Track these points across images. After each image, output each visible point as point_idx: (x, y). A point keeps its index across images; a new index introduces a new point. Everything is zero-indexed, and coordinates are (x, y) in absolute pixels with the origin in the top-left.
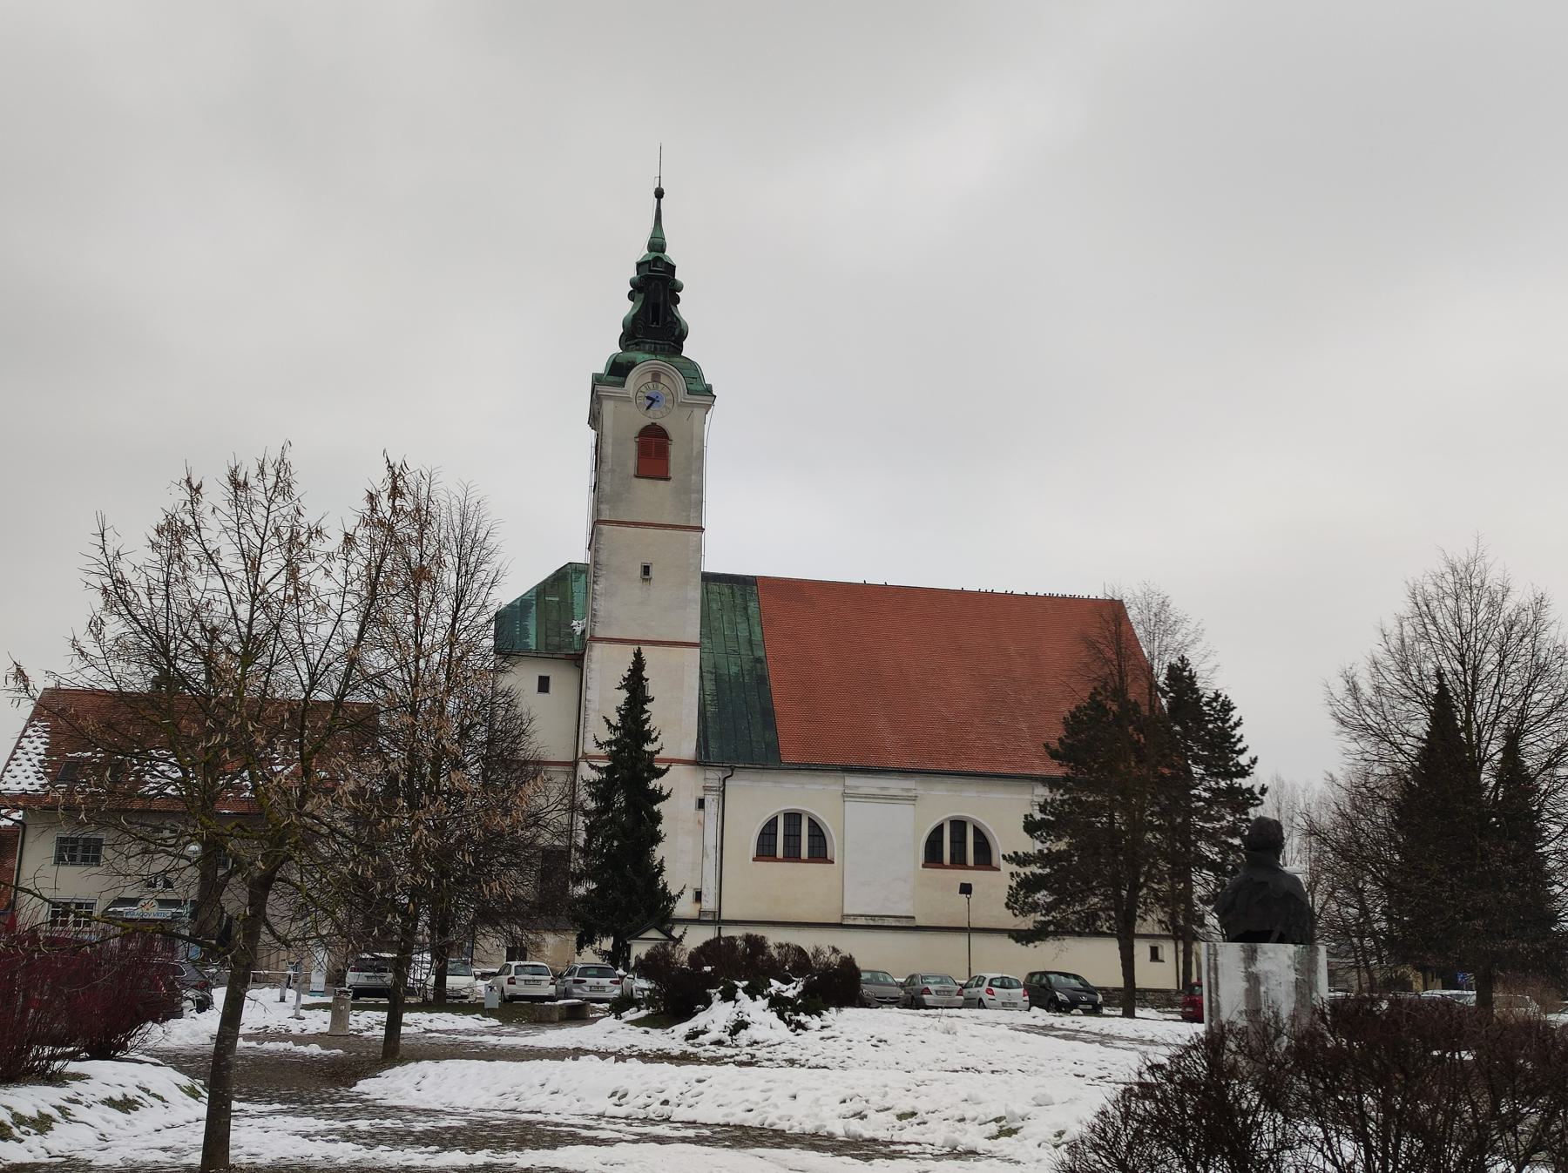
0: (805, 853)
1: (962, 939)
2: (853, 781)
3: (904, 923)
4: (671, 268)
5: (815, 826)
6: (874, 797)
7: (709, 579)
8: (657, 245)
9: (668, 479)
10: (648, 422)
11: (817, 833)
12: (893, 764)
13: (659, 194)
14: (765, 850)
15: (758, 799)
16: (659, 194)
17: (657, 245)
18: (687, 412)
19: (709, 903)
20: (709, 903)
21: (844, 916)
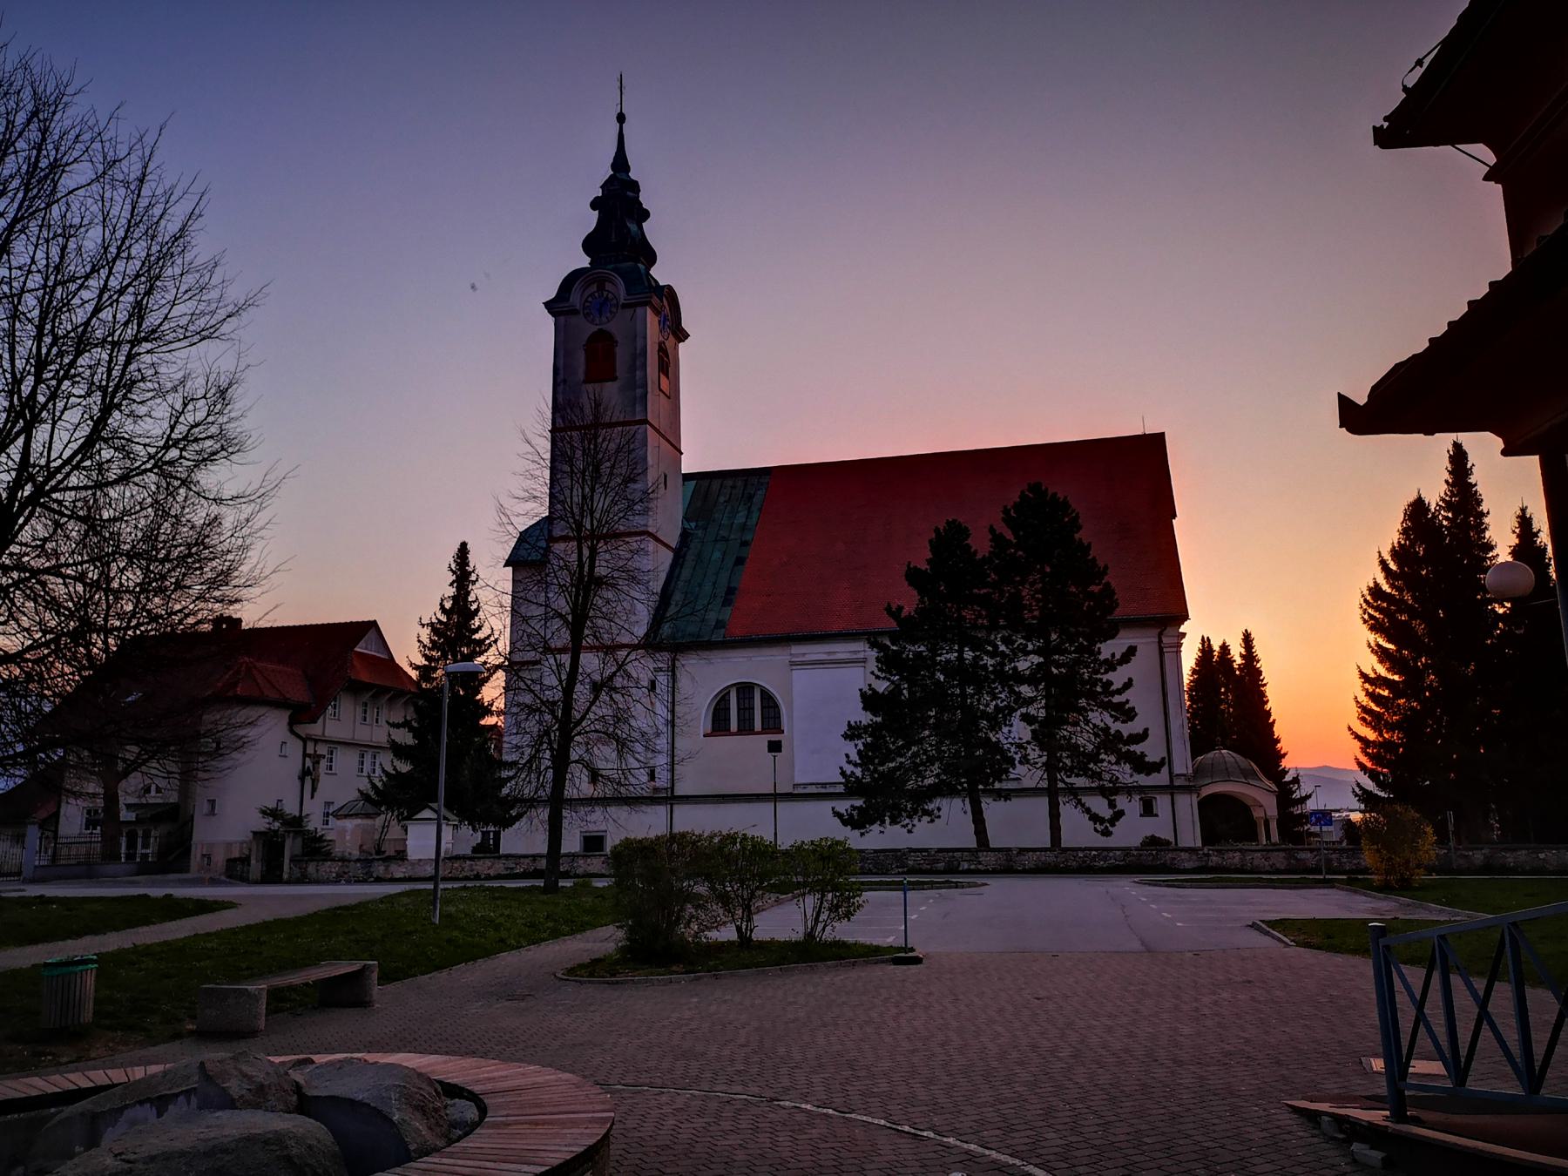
0: (734, 726)
1: (768, 807)
2: (798, 650)
3: (813, 790)
4: (635, 186)
5: (767, 698)
6: (821, 662)
7: (688, 477)
8: (620, 162)
9: (1147, 455)
10: (618, 338)
11: (769, 702)
12: (835, 629)
13: (621, 118)
14: (719, 725)
15: (706, 678)
16: (621, 118)
17: (620, 162)
18: (629, 312)
19: (662, 780)
20: (662, 780)
21: (795, 786)
